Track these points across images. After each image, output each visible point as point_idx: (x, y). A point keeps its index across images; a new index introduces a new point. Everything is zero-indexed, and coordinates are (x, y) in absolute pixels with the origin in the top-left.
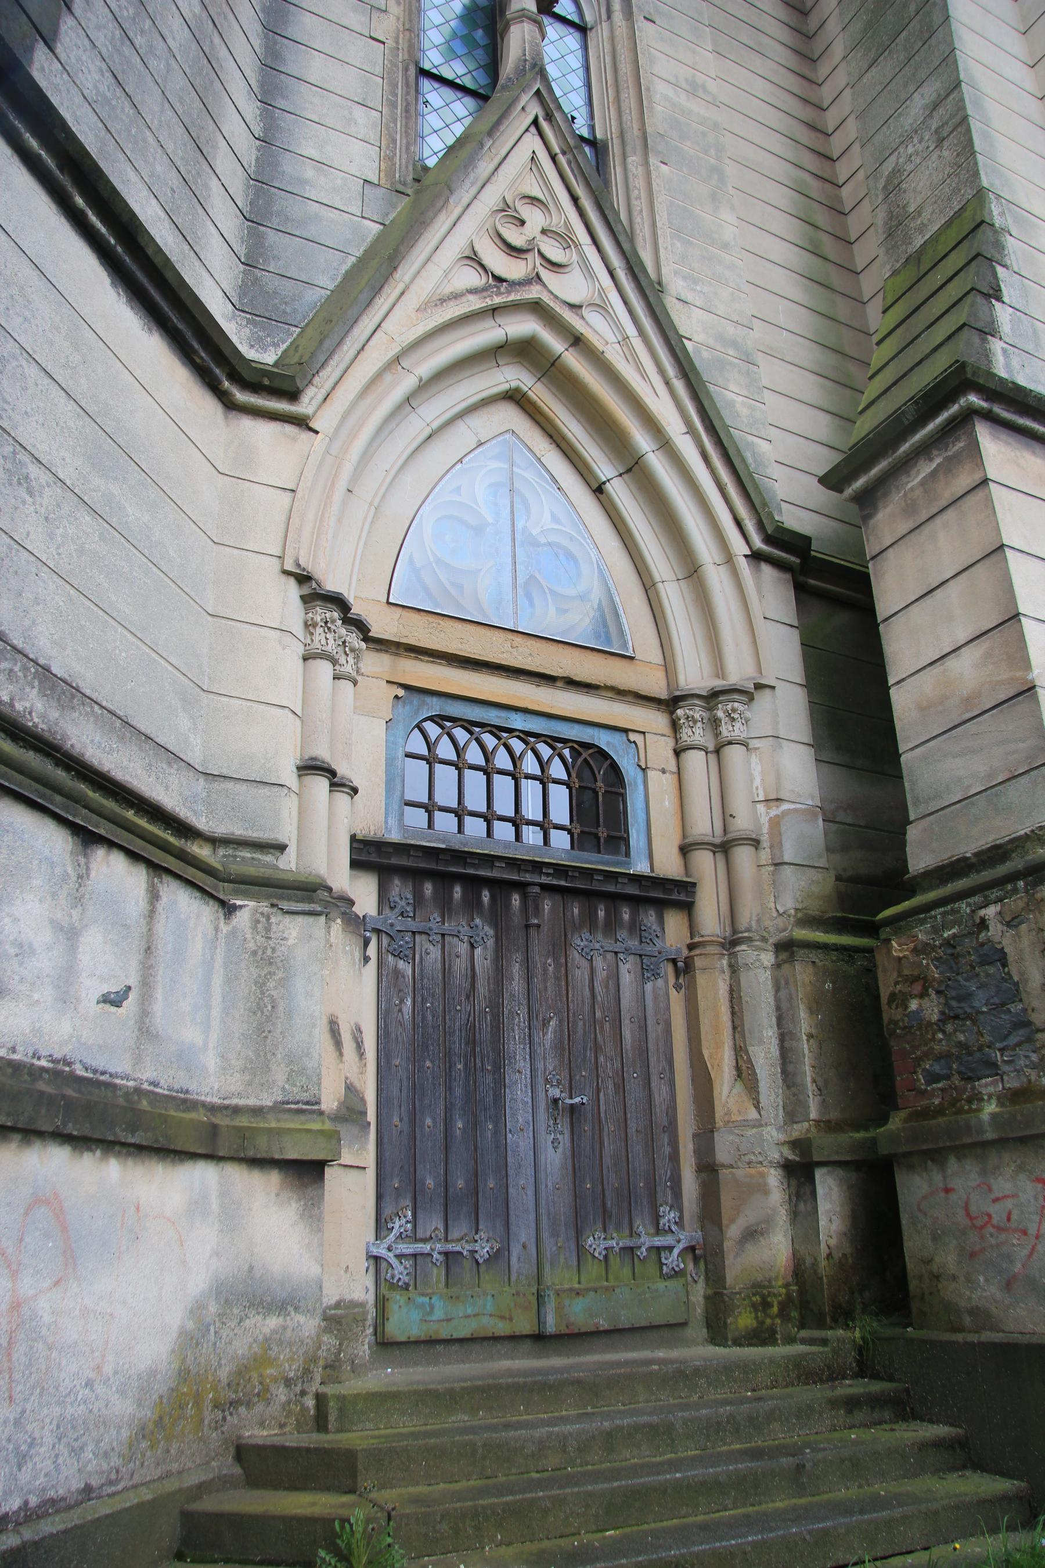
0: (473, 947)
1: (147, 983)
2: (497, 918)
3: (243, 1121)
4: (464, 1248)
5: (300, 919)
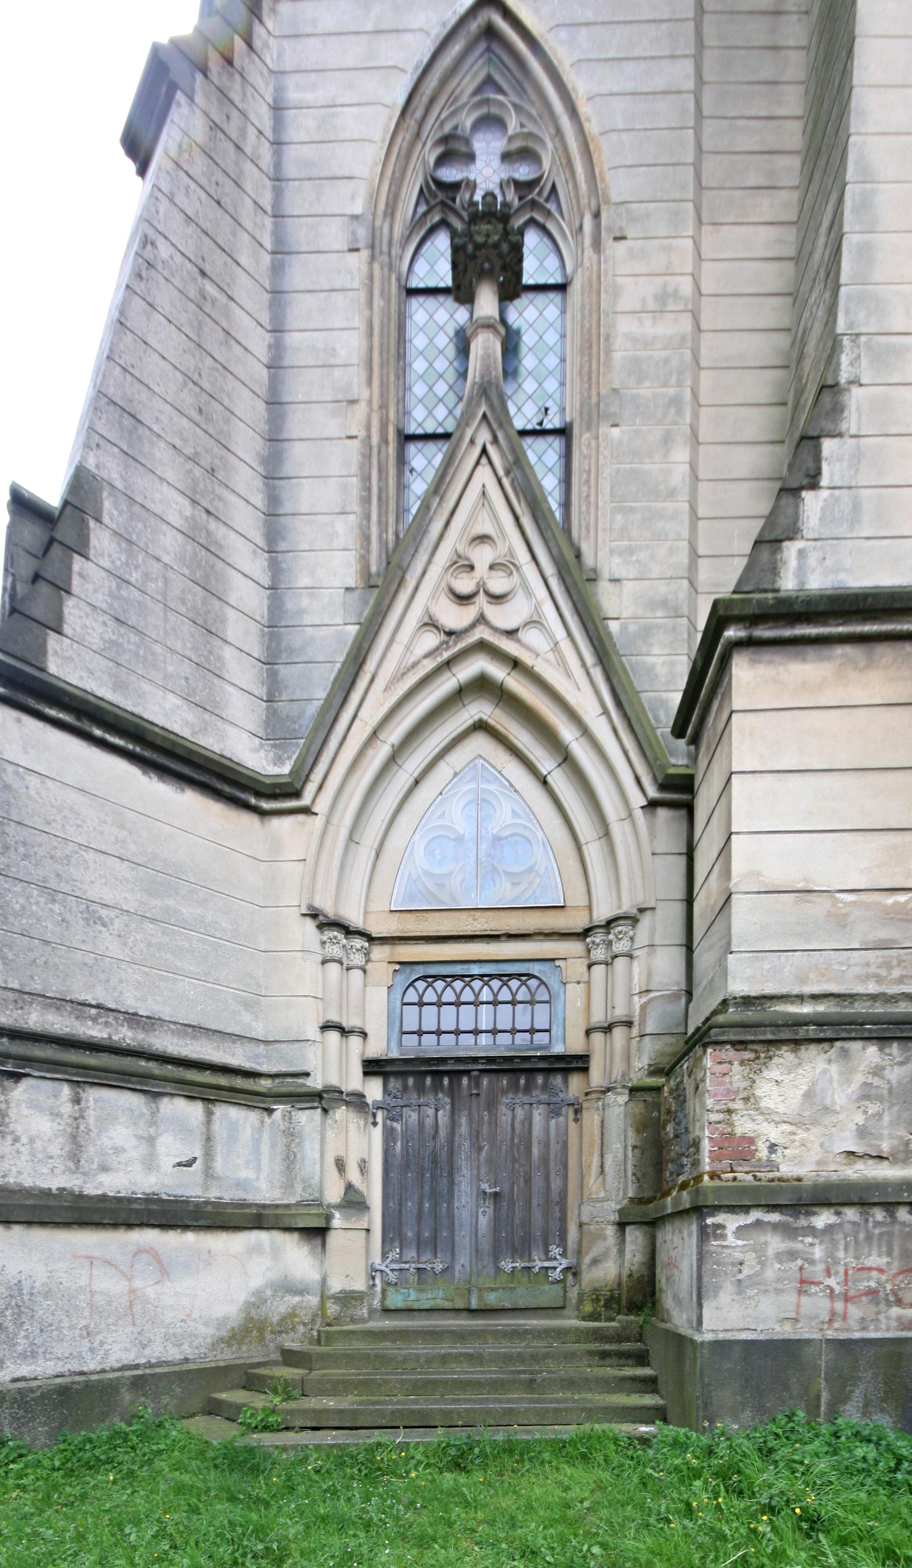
0: (437, 1110)
1: (209, 1154)
2: (452, 1093)
3: (280, 1211)
4: (428, 1266)
5: (307, 1112)
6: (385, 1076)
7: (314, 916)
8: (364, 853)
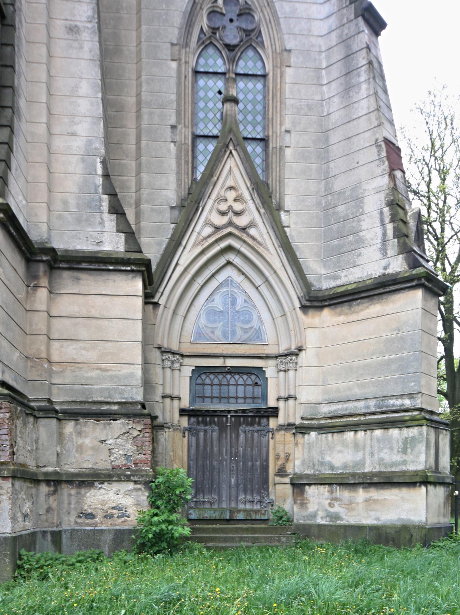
6: (190, 416)
7: (159, 348)
8: (179, 320)
